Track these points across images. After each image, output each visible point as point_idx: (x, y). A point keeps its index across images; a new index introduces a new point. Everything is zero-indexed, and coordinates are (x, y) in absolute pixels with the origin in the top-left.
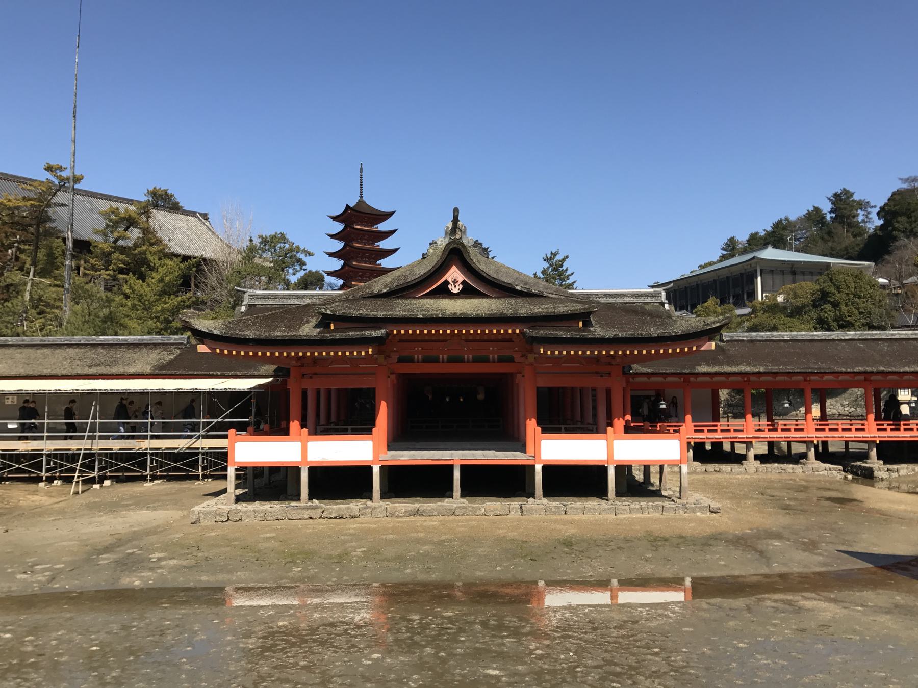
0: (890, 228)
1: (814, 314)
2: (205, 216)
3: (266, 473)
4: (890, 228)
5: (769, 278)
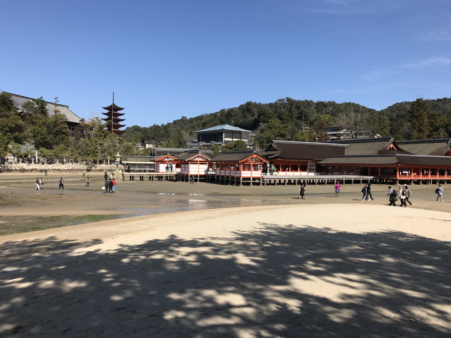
2: (67, 106)
3: (385, 111)
4: (259, 118)
5: (226, 134)
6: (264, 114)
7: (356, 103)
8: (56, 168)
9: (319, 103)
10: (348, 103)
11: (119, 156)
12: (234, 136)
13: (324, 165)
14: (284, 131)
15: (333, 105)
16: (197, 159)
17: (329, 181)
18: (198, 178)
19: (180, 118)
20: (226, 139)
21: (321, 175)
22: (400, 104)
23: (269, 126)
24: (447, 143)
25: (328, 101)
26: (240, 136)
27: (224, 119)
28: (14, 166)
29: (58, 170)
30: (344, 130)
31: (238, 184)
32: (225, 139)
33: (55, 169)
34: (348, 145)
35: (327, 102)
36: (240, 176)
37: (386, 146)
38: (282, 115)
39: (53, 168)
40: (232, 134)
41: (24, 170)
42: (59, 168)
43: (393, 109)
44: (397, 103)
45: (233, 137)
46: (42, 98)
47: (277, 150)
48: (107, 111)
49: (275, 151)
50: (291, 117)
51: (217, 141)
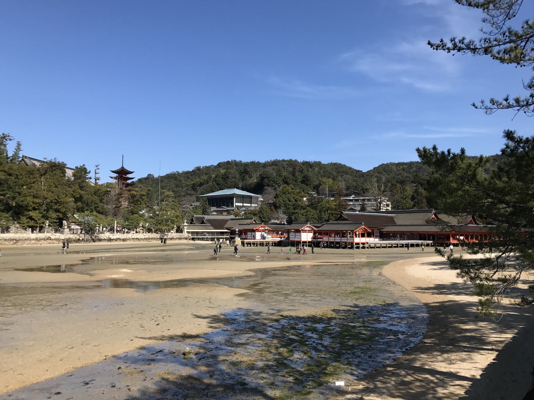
0: (263, 182)
1: (259, 215)
4: (263, 182)
5: (237, 198)
6: (268, 178)
7: (343, 163)
8: (135, 238)
9: (304, 163)
10: (334, 164)
11: (187, 224)
12: (244, 201)
13: (385, 232)
14: (298, 197)
15: (319, 165)
16: (306, 229)
19: (145, 176)
20: (237, 204)
21: (383, 240)
22: (386, 165)
23: (284, 192)
25: (314, 161)
26: (250, 200)
27: (221, 181)
28: (102, 236)
29: (137, 239)
30: (353, 196)
31: (352, 248)
32: (236, 204)
34: (395, 215)
35: (313, 162)
36: (354, 242)
38: (287, 179)
40: (242, 199)
41: (110, 239)
42: (138, 237)
43: (380, 171)
44: (383, 164)
45: (243, 201)
46: (85, 166)
47: (348, 220)
48: (115, 175)
49: (345, 220)
50: (296, 181)
51: (228, 206)
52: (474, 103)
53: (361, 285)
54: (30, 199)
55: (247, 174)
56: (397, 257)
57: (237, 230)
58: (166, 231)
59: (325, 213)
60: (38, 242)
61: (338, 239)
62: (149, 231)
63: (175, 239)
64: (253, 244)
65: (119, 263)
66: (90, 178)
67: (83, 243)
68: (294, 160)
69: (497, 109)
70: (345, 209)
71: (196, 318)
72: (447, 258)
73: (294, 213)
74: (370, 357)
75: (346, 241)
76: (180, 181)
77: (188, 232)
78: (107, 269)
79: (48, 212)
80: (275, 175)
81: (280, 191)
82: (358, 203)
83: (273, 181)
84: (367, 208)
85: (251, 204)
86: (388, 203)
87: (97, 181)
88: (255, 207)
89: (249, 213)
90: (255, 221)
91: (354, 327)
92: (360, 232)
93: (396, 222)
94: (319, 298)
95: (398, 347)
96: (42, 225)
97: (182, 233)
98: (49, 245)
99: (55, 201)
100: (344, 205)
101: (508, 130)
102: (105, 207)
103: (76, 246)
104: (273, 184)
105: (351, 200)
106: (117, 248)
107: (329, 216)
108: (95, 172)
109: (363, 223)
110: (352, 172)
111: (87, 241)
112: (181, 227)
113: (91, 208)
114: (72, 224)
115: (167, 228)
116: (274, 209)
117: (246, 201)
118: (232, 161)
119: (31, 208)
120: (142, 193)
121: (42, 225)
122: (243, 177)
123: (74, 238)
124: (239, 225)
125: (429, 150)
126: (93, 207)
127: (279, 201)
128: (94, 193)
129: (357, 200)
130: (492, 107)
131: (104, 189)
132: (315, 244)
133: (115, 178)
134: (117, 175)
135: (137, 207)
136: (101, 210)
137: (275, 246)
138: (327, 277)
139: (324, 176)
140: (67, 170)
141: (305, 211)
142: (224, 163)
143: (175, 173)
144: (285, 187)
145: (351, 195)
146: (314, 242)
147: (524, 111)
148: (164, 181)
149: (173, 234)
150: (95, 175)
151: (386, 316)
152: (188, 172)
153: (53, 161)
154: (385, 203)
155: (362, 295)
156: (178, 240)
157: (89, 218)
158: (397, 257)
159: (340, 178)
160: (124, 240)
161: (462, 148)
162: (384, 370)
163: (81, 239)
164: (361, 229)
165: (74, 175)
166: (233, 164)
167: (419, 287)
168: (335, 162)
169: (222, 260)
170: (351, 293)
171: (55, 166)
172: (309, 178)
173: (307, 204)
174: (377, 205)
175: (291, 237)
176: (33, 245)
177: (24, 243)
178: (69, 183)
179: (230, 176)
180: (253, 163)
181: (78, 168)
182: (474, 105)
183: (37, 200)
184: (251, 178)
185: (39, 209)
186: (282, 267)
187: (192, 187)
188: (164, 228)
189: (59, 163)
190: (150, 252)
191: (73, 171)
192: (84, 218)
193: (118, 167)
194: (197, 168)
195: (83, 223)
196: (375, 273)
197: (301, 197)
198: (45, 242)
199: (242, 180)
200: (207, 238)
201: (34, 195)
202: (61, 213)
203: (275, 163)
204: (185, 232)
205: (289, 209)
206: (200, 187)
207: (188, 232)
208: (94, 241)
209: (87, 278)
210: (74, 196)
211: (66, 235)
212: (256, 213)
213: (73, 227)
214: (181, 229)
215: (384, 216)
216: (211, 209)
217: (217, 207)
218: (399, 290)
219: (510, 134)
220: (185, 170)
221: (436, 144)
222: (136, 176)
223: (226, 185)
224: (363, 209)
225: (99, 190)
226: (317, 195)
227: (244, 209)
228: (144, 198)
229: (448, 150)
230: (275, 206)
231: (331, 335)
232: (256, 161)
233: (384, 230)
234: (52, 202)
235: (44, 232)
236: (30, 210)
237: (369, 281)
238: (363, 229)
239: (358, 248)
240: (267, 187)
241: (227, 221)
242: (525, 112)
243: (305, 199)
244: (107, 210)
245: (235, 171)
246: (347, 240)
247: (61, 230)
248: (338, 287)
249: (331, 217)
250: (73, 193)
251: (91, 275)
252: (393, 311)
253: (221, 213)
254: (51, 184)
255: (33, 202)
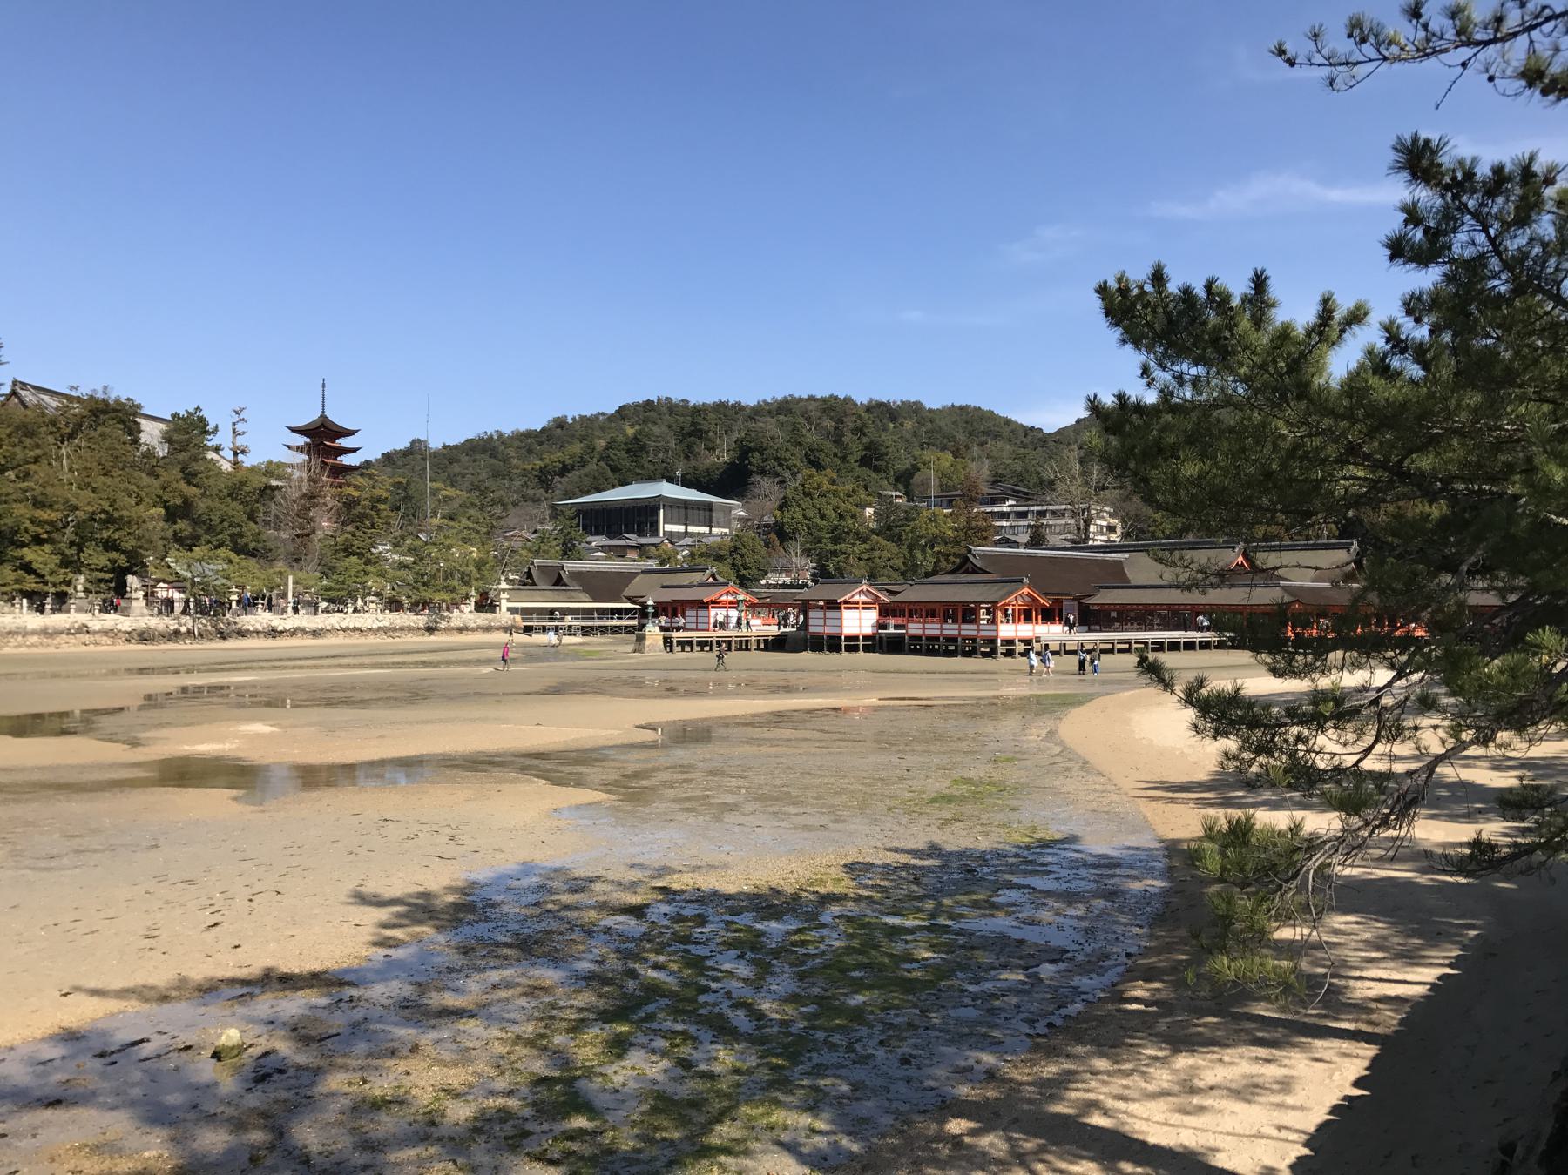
1: (730, 560)
5: (669, 511)
6: (761, 450)
7: (985, 407)
10: (961, 408)
11: (508, 587)
12: (690, 517)
13: (1096, 608)
14: (849, 506)
15: (915, 412)
16: (856, 598)
17: (708, 648)
18: (861, 643)
19: (404, 444)
20: (669, 527)
21: (1090, 631)
24: (1349, 551)
29: (355, 629)
30: (1011, 502)
31: (992, 653)
33: (348, 629)
34: (1127, 556)
37: (1228, 561)
39: (344, 625)
40: (684, 511)
42: (358, 625)
45: (686, 519)
48: (302, 440)
50: (844, 459)
51: (641, 534)
52: (1280, 45)
53: (979, 771)
54: (22, 511)
55: (700, 438)
56: (1120, 682)
57: (650, 603)
58: (444, 605)
59: (924, 552)
60: (49, 641)
61: (950, 629)
62: (394, 605)
63: (473, 630)
64: (699, 643)
65: (255, 704)
66: (217, 449)
67: (188, 641)
68: (842, 397)
69: (1378, 63)
70: (984, 540)
71: (356, 903)
72: (1182, 695)
73: (834, 553)
74: (905, 1061)
75: (975, 633)
76: (506, 460)
77: (513, 611)
78: (199, 724)
79: (81, 550)
80: (781, 441)
81: (796, 489)
82: (1026, 523)
83: (777, 459)
84: (1048, 537)
85: (711, 527)
86: (1113, 521)
87: (240, 457)
88: (722, 536)
89: (701, 555)
90: (713, 576)
91: (894, 932)
92: (1017, 607)
93: (1130, 576)
94: (824, 820)
95: (1022, 1016)
96: (64, 588)
97: (494, 612)
98: (84, 648)
99: (103, 516)
100: (980, 530)
101: (1415, 138)
102: (263, 537)
103: (164, 651)
104: (776, 468)
105: (1003, 515)
106: (288, 656)
107: (938, 561)
108: (234, 431)
109: (1026, 580)
110: (1012, 431)
111: (201, 635)
112: (492, 594)
113: (220, 537)
114: (161, 585)
115: (446, 596)
116: (778, 543)
117: (696, 518)
118: (659, 399)
119: (26, 538)
120: (378, 492)
121: (64, 588)
122: (689, 447)
123: (161, 627)
124: (663, 587)
125: (1141, 288)
126: (224, 536)
127: (793, 519)
128: (230, 495)
129: (1022, 515)
130: (1357, 57)
131: (259, 481)
132: (885, 644)
133: (300, 449)
134: (308, 440)
135: (361, 534)
136: (252, 545)
137: (766, 649)
138: (883, 745)
139: (928, 444)
140: (143, 422)
141: (867, 546)
142: (637, 405)
143: (491, 437)
144: (811, 477)
145: (1003, 501)
146: (881, 638)
147: (1486, 76)
148: (458, 461)
149: (467, 614)
150: (234, 438)
151: (1020, 887)
152: (529, 434)
153: (100, 395)
154: (1105, 523)
155: (968, 809)
156: (480, 632)
157: (212, 566)
158: (1120, 682)
159: (976, 450)
160: (316, 633)
161: (1256, 272)
162: (933, 1128)
163: (183, 629)
164: (1019, 599)
165: (168, 439)
166: (664, 410)
167: (1162, 782)
168: (964, 404)
169: (583, 693)
170: (934, 800)
171: (104, 412)
172: (883, 450)
173: (874, 525)
174: (1079, 529)
175: (811, 622)
176: (34, 650)
177: (6, 644)
178: (151, 465)
179: (651, 444)
180: (720, 407)
181: (179, 419)
182: (1281, 52)
183: (44, 515)
184: (712, 449)
185: (50, 541)
186: (754, 715)
187: (540, 478)
188: (437, 597)
189: (117, 401)
190: (382, 668)
191: (162, 426)
192: (189, 566)
193: (309, 417)
194: (555, 420)
195: (188, 585)
196: (1036, 732)
197: (857, 505)
198: (72, 640)
199: (687, 457)
200: (570, 627)
201: (34, 498)
202: (123, 552)
203: (784, 408)
204: (504, 609)
205: (820, 542)
206: (562, 476)
207: (513, 611)
208: (223, 636)
209: (118, 753)
210: (166, 502)
211: (138, 615)
212: (722, 553)
213: (162, 593)
214: (492, 601)
215: (1096, 561)
216: (589, 543)
217: (610, 535)
218: (1095, 791)
219: (1420, 156)
220: (522, 428)
221: (1163, 262)
222: (367, 447)
223: (637, 470)
224: (1037, 540)
225: (243, 483)
226: (905, 499)
227: (688, 541)
228: (382, 507)
229: (1208, 280)
230: (782, 534)
231: (803, 963)
232: (732, 402)
233: (1091, 601)
234: (95, 520)
235: (68, 611)
236: (23, 545)
237: (1008, 760)
238: (1027, 599)
239: (1010, 653)
240: (758, 478)
241: (632, 575)
242: (1491, 79)
243: (869, 511)
244: (270, 545)
245: (664, 429)
246: (979, 630)
247: (123, 603)
248: (901, 779)
249: (943, 564)
250: (161, 492)
251: (135, 743)
252: (1049, 868)
253: (621, 553)
254: (89, 465)
255: (32, 521)
